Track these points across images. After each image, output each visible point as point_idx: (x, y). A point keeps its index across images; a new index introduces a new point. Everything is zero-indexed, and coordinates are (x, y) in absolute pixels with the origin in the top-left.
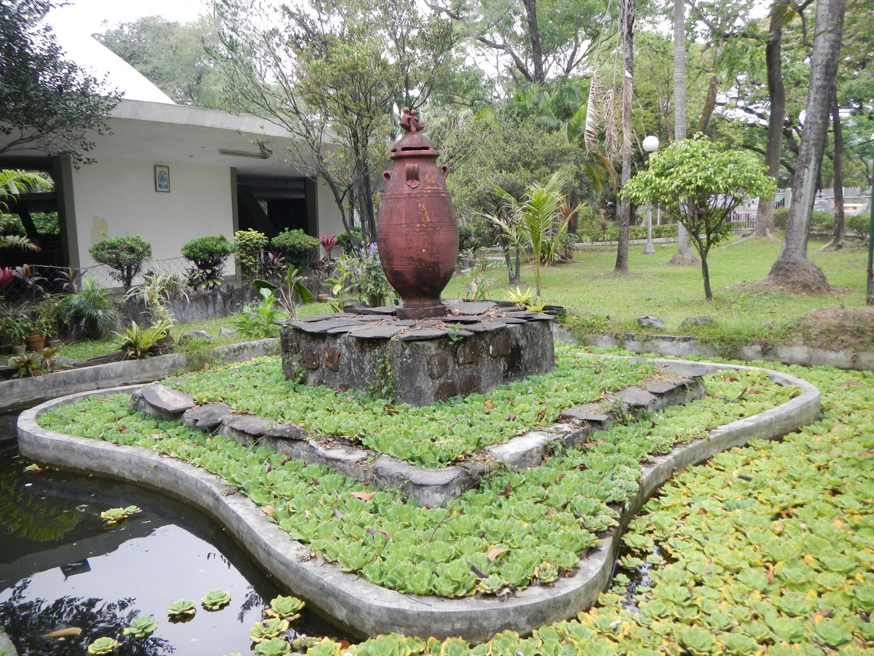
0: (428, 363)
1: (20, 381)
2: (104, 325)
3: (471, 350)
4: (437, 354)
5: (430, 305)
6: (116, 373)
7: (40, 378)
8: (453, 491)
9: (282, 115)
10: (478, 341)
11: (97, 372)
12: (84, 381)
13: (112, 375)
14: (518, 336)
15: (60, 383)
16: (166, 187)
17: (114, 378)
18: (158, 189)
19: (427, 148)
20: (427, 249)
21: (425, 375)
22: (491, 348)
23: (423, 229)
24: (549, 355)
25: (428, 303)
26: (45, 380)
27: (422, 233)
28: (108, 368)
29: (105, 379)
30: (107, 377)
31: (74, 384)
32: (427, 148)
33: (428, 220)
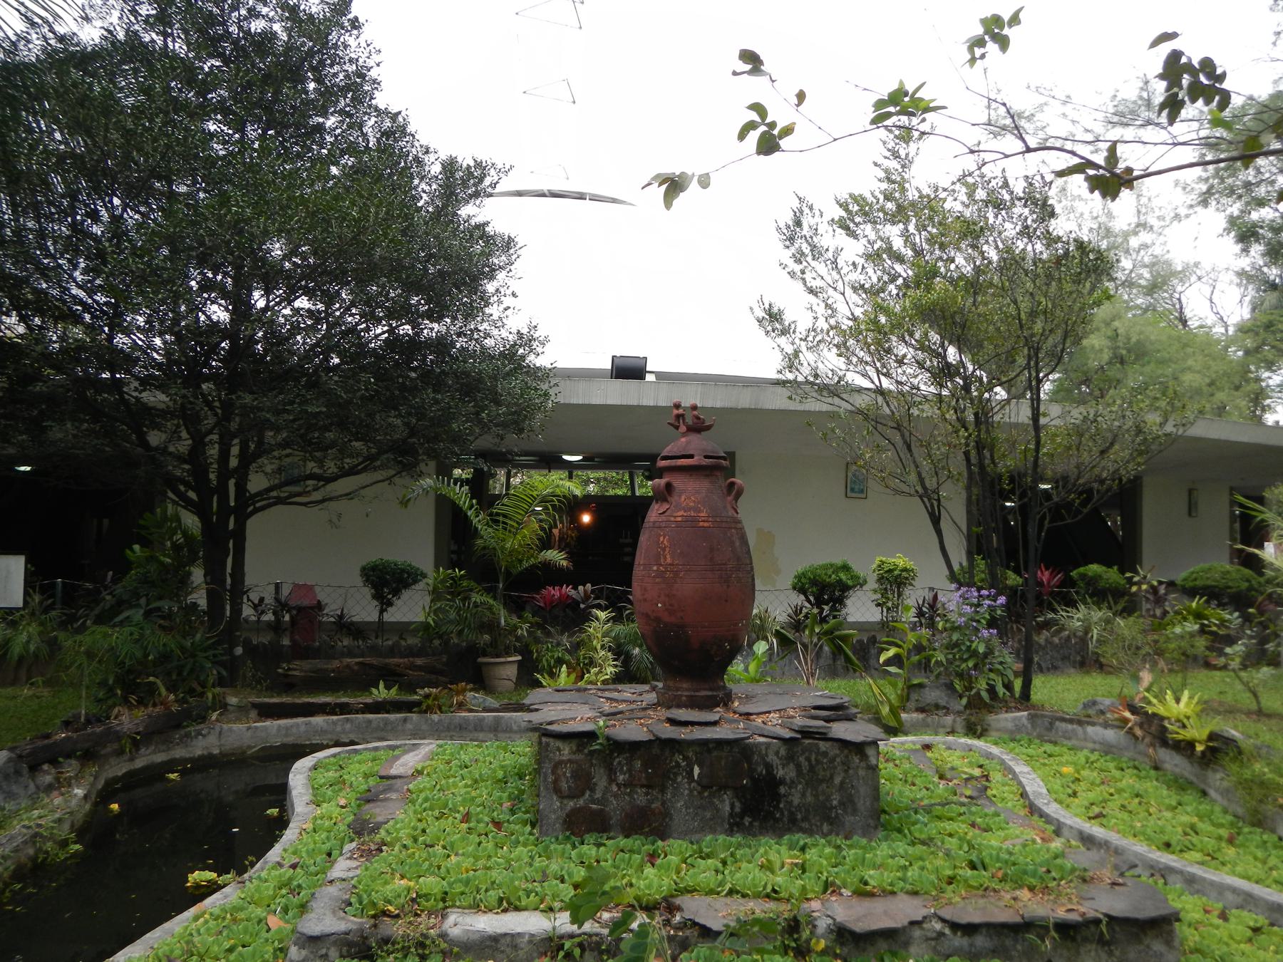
0: (553, 773)
1: (414, 716)
2: (638, 668)
3: (645, 765)
4: (570, 761)
5: (687, 690)
6: (519, 726)
7: (435, 717)
8: (324, 951)
9: (1276, 395)
10: (667, 753)
11: (497, 720)
12: (482, 730)
13: (515, 728)
14: (772, 758)
15: (456, 727)
16: (862, 491)
17: (516, 732)
18: (849, 494)
19: (691, 456)
20: (664, 604)
21: (547, 789)
22: (697, 770)
23: (660, 574)
24: (863, 804)
25: (685, 686)
26: (440, 721)
27: (657, 580)
28: (510, 718)
29: (505, 731)
30: (509, 730)
31: (471, 731)
32: (691, 456)
33: (669, 560)
